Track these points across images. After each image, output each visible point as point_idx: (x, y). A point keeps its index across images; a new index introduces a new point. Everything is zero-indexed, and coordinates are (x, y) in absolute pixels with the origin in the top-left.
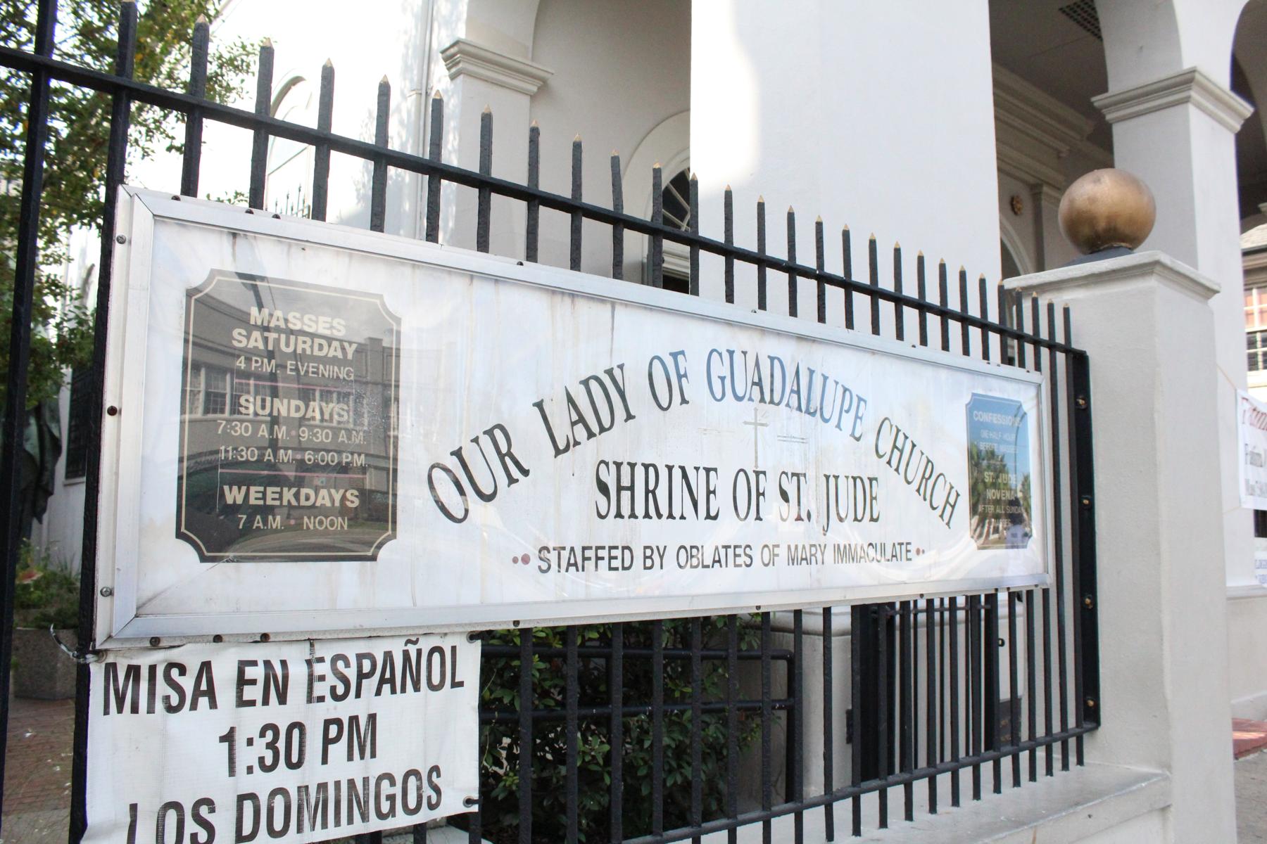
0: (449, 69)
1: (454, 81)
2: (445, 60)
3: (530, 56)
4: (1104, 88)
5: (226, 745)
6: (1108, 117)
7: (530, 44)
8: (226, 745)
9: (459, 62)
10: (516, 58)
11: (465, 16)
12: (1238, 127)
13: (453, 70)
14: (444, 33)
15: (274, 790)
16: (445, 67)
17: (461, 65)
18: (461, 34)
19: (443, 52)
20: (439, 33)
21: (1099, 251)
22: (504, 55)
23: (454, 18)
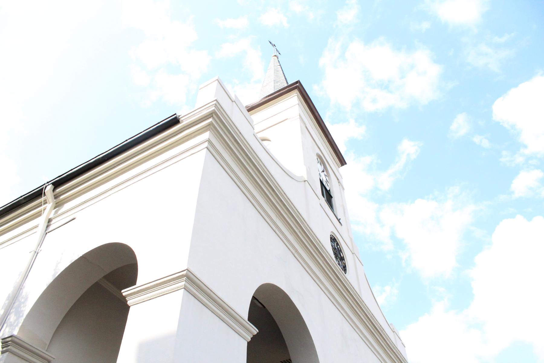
0: (3, 348)
1: (3, 354)
2: (2, 343)
3: (46, 348)
4: (133, 281)
5: (339, 218)
6: (129, 303)
7: (48, 343)
8: (339, 218)
9: (9, 346)
10: (38, 348)
11: (20, 324)
12: (249, 339)
13: (4, 349)
14: (7, 330)
15: (322, 195)
16: (1, 347)
17: (9, 347)
18: (15, 333)
19: (3, 339)
20: (5, 329)
21: (343, 257)
22: (33, 346)
23: (15, 324)
